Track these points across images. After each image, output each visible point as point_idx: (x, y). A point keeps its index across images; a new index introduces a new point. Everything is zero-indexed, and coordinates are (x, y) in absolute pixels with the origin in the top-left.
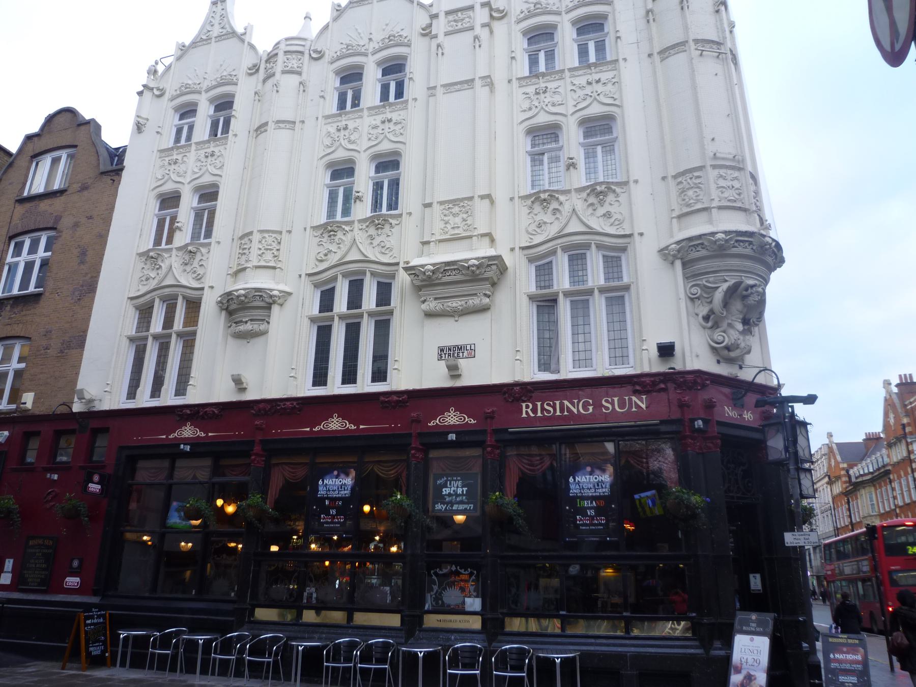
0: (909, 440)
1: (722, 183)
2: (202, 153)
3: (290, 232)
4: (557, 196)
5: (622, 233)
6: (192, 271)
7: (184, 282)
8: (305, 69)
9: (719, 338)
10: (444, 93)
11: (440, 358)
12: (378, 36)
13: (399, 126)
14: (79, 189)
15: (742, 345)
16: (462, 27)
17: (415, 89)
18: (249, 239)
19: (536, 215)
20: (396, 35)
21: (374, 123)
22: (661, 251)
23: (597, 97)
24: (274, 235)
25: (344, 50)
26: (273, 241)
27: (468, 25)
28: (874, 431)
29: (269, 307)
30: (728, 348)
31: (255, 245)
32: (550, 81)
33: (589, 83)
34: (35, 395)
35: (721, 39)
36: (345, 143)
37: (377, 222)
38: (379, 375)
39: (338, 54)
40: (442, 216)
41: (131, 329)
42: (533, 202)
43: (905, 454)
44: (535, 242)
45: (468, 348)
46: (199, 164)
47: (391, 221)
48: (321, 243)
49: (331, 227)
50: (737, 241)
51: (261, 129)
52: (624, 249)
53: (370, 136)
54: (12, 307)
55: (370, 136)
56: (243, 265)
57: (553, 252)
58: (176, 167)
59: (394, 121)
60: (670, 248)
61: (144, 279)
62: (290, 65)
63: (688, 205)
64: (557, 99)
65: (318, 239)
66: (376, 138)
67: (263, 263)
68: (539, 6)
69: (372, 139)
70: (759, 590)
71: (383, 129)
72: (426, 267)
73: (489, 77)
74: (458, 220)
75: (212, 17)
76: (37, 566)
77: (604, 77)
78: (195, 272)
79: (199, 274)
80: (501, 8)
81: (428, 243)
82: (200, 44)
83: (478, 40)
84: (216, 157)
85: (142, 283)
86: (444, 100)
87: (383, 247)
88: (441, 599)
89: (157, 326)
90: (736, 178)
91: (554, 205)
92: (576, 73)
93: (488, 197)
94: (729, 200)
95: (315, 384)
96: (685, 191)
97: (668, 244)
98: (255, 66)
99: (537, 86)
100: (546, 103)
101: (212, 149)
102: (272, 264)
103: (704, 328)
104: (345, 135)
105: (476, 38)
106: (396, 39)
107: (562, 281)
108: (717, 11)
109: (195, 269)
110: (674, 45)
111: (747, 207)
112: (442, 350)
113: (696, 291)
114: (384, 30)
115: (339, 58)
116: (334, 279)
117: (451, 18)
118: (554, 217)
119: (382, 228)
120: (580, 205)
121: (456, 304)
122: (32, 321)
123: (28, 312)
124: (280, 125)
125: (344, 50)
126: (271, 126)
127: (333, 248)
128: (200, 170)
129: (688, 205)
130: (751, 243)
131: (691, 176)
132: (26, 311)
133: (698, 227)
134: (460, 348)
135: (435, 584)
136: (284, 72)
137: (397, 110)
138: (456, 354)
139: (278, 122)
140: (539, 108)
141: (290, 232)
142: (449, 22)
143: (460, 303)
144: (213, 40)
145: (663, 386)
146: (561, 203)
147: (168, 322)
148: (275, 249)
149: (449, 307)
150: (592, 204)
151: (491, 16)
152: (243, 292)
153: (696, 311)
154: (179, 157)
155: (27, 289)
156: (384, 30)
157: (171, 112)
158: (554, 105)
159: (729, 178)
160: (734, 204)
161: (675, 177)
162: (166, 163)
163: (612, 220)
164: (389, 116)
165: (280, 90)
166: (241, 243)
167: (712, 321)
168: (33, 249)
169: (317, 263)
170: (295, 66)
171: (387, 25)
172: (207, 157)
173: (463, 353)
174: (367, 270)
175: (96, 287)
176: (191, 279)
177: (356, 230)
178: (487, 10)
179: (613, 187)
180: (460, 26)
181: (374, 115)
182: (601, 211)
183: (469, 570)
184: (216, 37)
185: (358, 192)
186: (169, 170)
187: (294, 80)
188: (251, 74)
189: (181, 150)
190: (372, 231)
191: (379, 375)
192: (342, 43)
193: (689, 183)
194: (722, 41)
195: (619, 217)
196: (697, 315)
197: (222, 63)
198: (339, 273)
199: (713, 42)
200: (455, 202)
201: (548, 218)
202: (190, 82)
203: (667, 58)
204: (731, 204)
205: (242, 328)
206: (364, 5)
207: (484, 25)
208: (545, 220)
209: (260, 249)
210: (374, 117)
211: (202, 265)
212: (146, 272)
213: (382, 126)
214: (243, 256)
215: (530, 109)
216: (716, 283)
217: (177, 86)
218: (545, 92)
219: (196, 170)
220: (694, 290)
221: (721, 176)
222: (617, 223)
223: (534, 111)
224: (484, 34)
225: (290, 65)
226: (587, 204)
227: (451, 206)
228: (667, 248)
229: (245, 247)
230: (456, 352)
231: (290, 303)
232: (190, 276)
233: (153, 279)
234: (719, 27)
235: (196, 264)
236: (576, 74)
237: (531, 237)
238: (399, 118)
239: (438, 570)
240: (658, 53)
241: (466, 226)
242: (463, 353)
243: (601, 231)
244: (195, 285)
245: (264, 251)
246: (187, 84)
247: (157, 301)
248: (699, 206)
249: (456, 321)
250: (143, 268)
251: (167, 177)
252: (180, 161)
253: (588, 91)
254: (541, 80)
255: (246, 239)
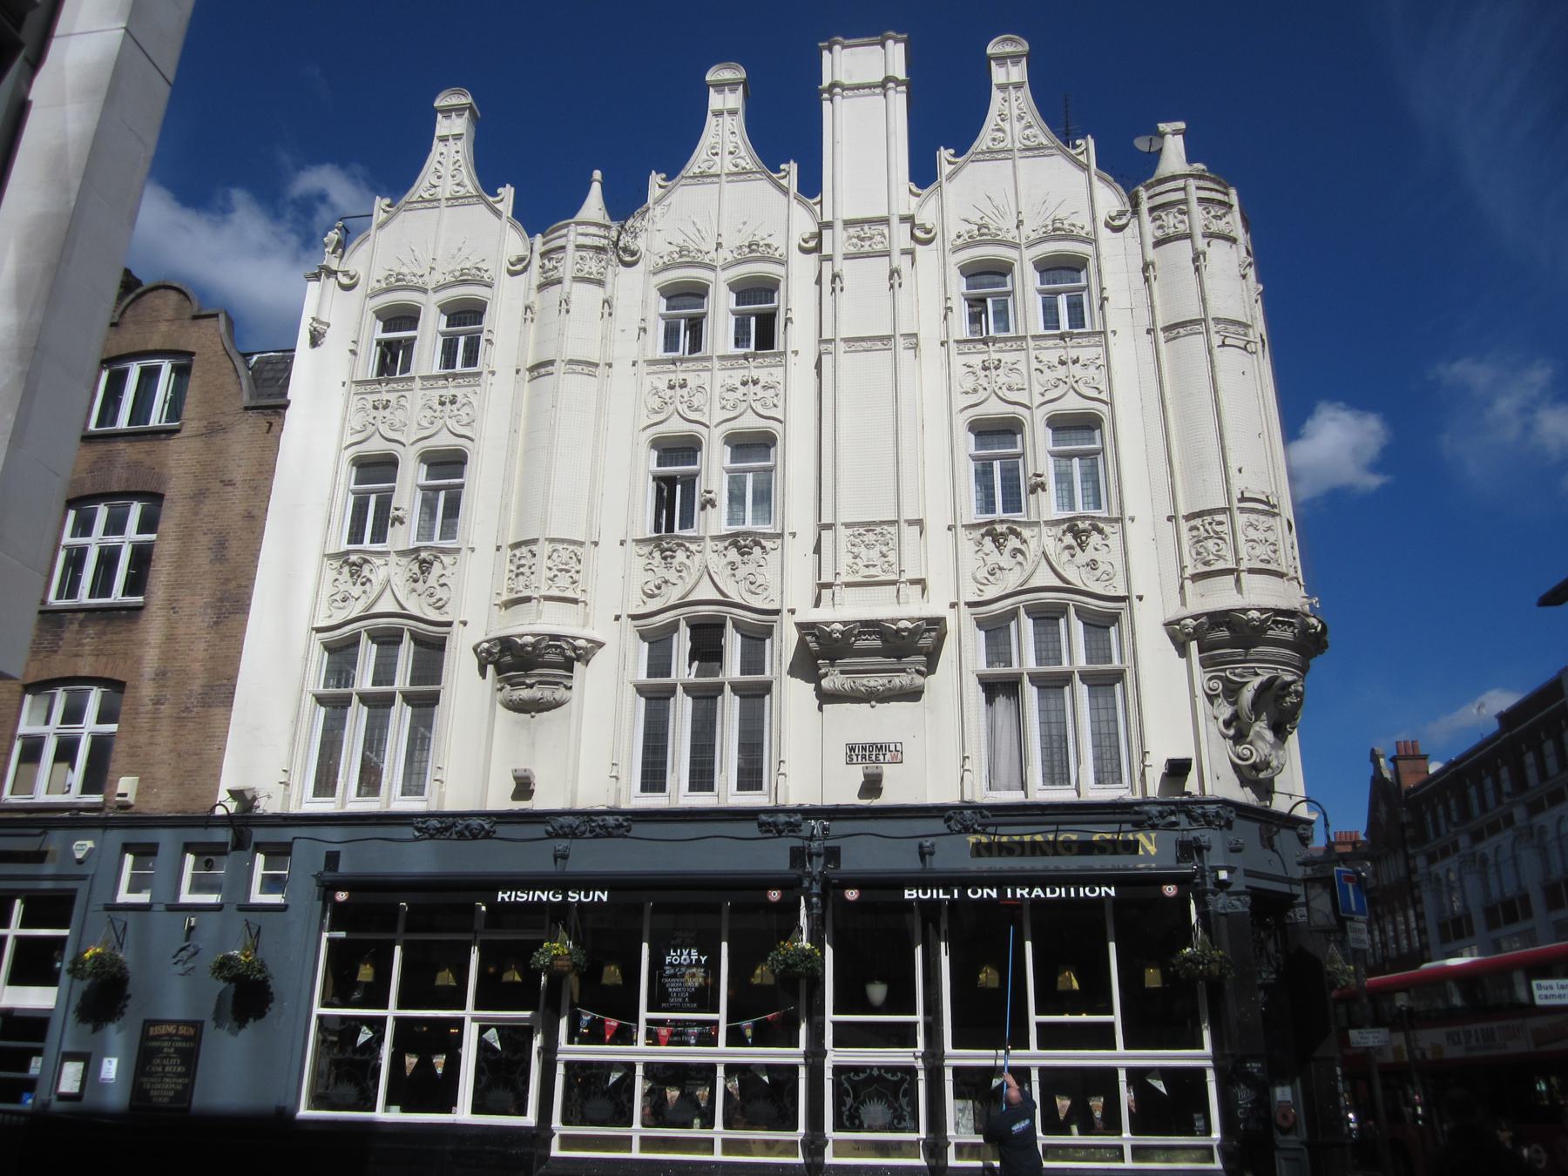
0: (1411, 851)
1: (1252, 534)
2: (435, 395)
3: (596, 544)
4: (1019, 529)
5: (1112, 593)
6: (428, 593)
7: (413, 610)
8: (609, 278)
9: (1245, 752)
10: (845, 352)
11: (850, 762)
12: (732, 240)
13: (771, 392)
14: (204, 431)
15: (1274, 763)
16: (870, 249)
17: (797, 335)
18: (531, 551)
19: (987, 555)
20: (761, 243)
21: (730, 382)
22: (1168, 624)
23: (1075, 385)
24: (571, 548)
25: (676, 256)
26: (571, 558)
27: (879, 247)
28: (1348, 830)
29: (568, 665)
30: (1254, 767)
31: (542, 563)
32: (1004, 351)
33: (1062, 363)
34: (140, 781)
35: (1250, 319)
36: (683, 408)
37: (742, 543)
38: (750, 777)
39: (666, 259)
40: (850, 547)
41: (316, 682)
42: (983, 536)
43: (1402, 872)
44: (987, 596)
45: (892, 748)
46: (429, 413)
47: (764, 542)
48: (649, 566)
49: (668, 543)
50: (1275, 622)
51: (540, 368)
52: (1114, 618)
53: (724, 402)
54: (82, 624)
55: (724, 402)
56: (521, 591)
57: (1013, 614)
58: (386, 413)
59: (762, 383)
60: (1183, 622)
61: (338, 597)
62: (586, 269)
63: (1207, 563)
64: (1015, 379)
65: (644, 561)
66: (734, 407)
67: (555, 593)
68: (984, 231)
69: (728, 407)
70: (1289, 1102)
71: (745, 394)
72: (833, 626)
73: (915, 335)
74: (874, 554)
75: (439, 162)
76: (167, 1069)
77: (1085, 354)
78: (431, 595)
79: (440, 599)
80: (929, 226)
81: (829, 586)
82: (419, 206)
83: (898, 275)
84: (458, 405)
85: (336, 604)
86: (848, 364)
87: (752, 583)
88: (859, 1117)
89: (364, 680)
90: (1269, 529)
91: (1013, 542)
92: (1043, 343)
93: (919, 523)
94: (1262, 561)
95: (645, 788)
96: (1201, 541)
97: (1180, 617)
98: (521, 260)
99: (985, 357)
100: (999, 384)
101: (453, 391)
102: (569, 594)
103: (1225, 736)
104: (682, 397)
105: (894, 273)
106: (760, 249)
107: (1026, 658)
108: (1244, 277)
109: (432, 590)
110: (1186, 322)
111: (1284, 570)
112: (852, 749)
113: (1216, 685)
114: (740, 231)
115: (666, 268)
116: (1013, 614)
117: (852, 231)
118: (1014, 561)
119: (750, 554)
120: (1052, 547)
121: (877, 682)
122: (126, 654)
123: (115, 637)
124: (574, 367)
125: (676, 256)
126: (559, 367)
127: (671, 575)
128: (432, 423)
129: (1207, 563)
130: (1291, 625)
131: (1210, 521)
132: (111, 633)
133: (1222, 596)
134: (880, 748)
135: (848, 1095)
136: (576, 279)
137: (767, 366)
138: (874, 758)
139: (571, 362)
140: (989, 390)
141: (596, 544)
142: (850, 238)
143: (881, 682)
144: (443, 203)
145: (1173, 819)
146: (1025, 541)
147: (384, 673)
148: (573, 570)
149: (863, 685)
150: (1069, 547)
151: (913, 236)
152: (530, 639)
153: (1216, 713)
154: (392, 397)
155: (108, 595)
156: (740, 231)
157: (370, 317)
158: (1010, 389)
159: (1261, 528)
160: (1269, 567)
161: (1188, 518)
162: (369, 406)
163: (1098, 573)
164: (755, 374)
165: (572, 307)
166: (515, 555)
167: (1238, 730)
168: (116, 525)
169: (645, 598)
170: (594, 270)
171: (745, 223)
172: (442, 404)
173: (884, 755)
174: (728, 616)
175: (249, 605)
176: (425, 606)
177: (708, 550)
178: (907, 226)
179: (1101, 525)
180: (867, 249)
181: (729, 369)
182: (1081, 558)
183: (899, 1074)
184: (448, 199)
185: (709, 492)
186: (374, 418)
187: (595, 294)
188: (513, 274)
189: (395, 385)
190: (733, 554)
191: (750, 777)
192: (670, 243)
193: (1207, 531)
194: (1249, 323)
195: (1109, 569)
196: (1216, 718)
197: (460, 245)
198: (681, 617)
199: (1239, 323)
200: (869, 526)
201: (1005, 560)
202: (405, 270)
203: (1174, 338)
204: (1263, 566)
205: (525, 694)
206: (704, 183)
207: (905, 252)
208: (1001, 565)
209: (550, 569)
210: (730, 372)
211: (444, 585)
212: (342, 588)
213: (743, 389)
214: (521, 577)
215: (975, 391)
216: (1244, 677)
217: (382, 275)
218: (996, 368)
219: (425, 423)
220: (1213, 684)
221: (1251, 525)
222: (1105, 577)
223: (982, 395)
224: (903, 263)
225: (586, 269)
226: (1063, 545)
227: (862, 531)
228: (1178, 622)
229: (523, 562)
230: (874, 753)
231: (598, 659)
232: (425, 600)
233: (357, 599)
234: (1246, 299)
235: (432, 579)
236: (1043, 345)
237: (982, 587)
238: (770, 380)
239: (852, 1074)
240: (1162, 329)
241: (886, 565)
242: (884, 755)
243: (1084, 588)
244: (433, 615)
245: (556, 573)
246: (398, 274)
247: (364, 636)
248: (1220, 565)
249: (872, 707)
250: (336, 580)
251: (371, 429)
252: (393, 403)
253: (1061, 372)
254: (992, 348)
255: (524, 550)
